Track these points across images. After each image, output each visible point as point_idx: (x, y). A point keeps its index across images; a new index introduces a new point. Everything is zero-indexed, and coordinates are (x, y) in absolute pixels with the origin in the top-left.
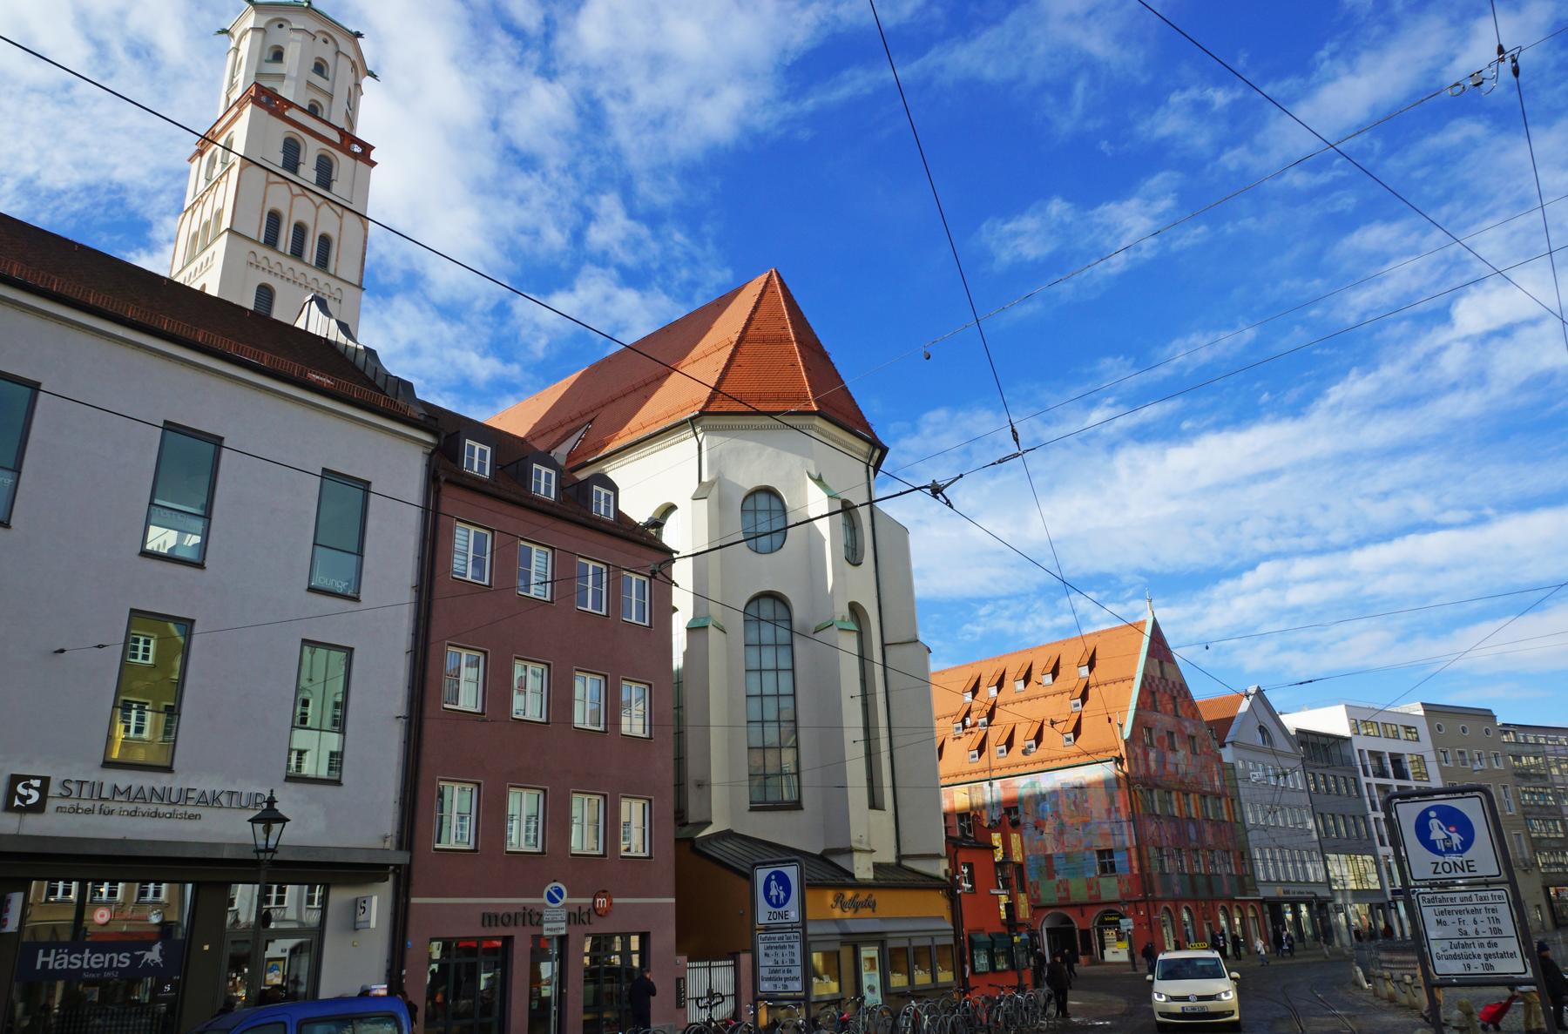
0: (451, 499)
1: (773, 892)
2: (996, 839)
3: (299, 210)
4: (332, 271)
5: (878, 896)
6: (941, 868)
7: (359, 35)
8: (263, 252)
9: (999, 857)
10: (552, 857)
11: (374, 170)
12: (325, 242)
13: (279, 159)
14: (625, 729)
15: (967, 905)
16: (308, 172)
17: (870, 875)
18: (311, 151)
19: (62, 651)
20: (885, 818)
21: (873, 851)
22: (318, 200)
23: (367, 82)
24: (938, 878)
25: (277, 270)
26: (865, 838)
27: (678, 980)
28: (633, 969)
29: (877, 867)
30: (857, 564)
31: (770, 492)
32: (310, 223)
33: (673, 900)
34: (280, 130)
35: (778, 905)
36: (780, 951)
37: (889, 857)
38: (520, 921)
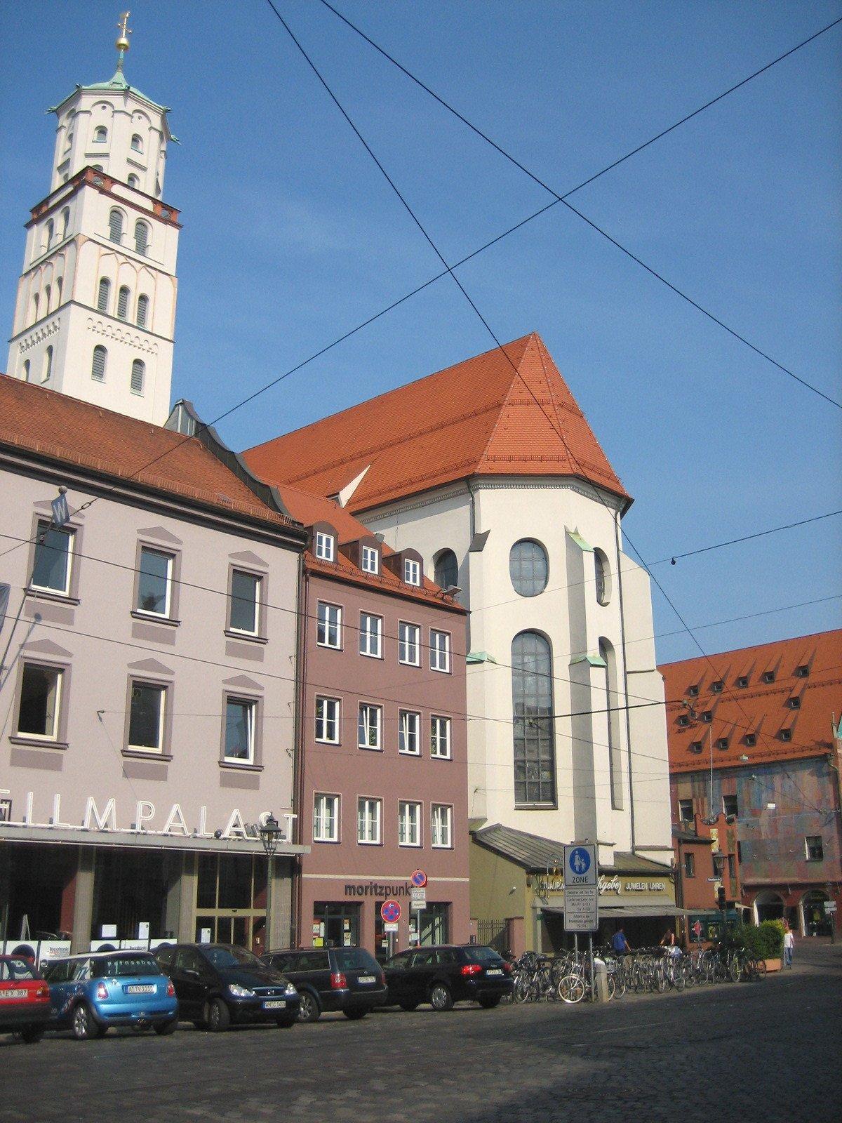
1: (577, 863)
6: (667, 858)
10: (388, 847)
13: (107, 232)
16: (129, 240)
22: (138, 266)
28: (175, 1012)
29: (617, 855)
32: (132, 287)
35: (580, 872)
37: (626, 848)
38: (369, 890)
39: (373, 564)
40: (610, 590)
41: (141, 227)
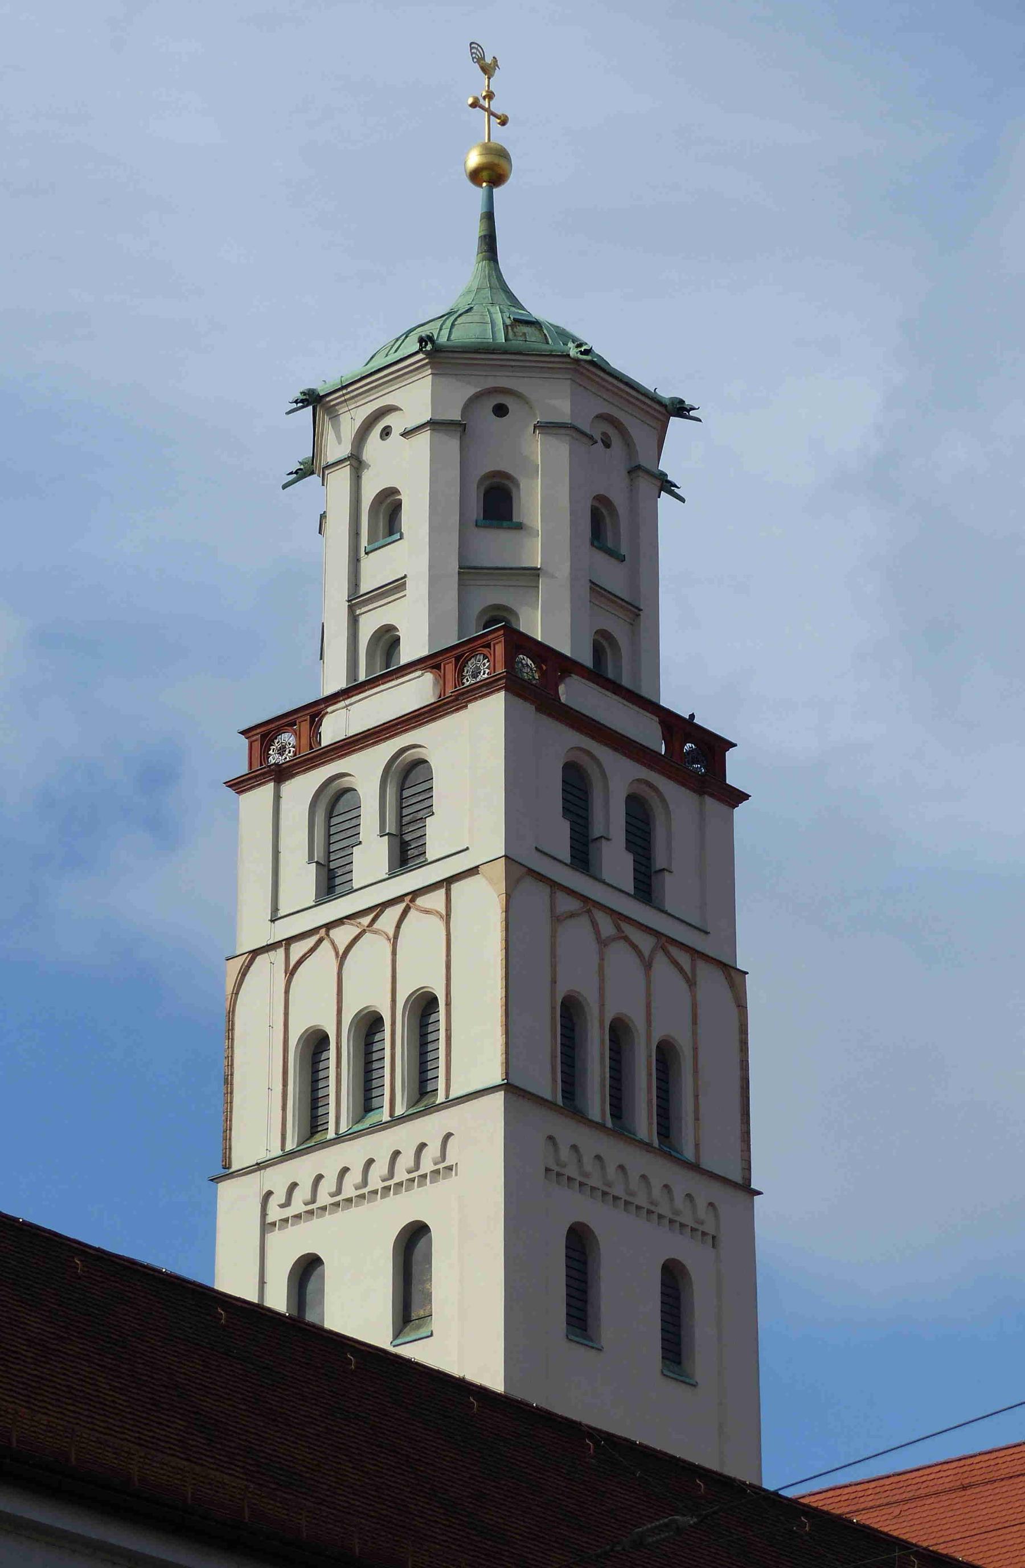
8: (568, 1132)
11: (740, 812)
12: (666, 1056)
16: (616, 862)
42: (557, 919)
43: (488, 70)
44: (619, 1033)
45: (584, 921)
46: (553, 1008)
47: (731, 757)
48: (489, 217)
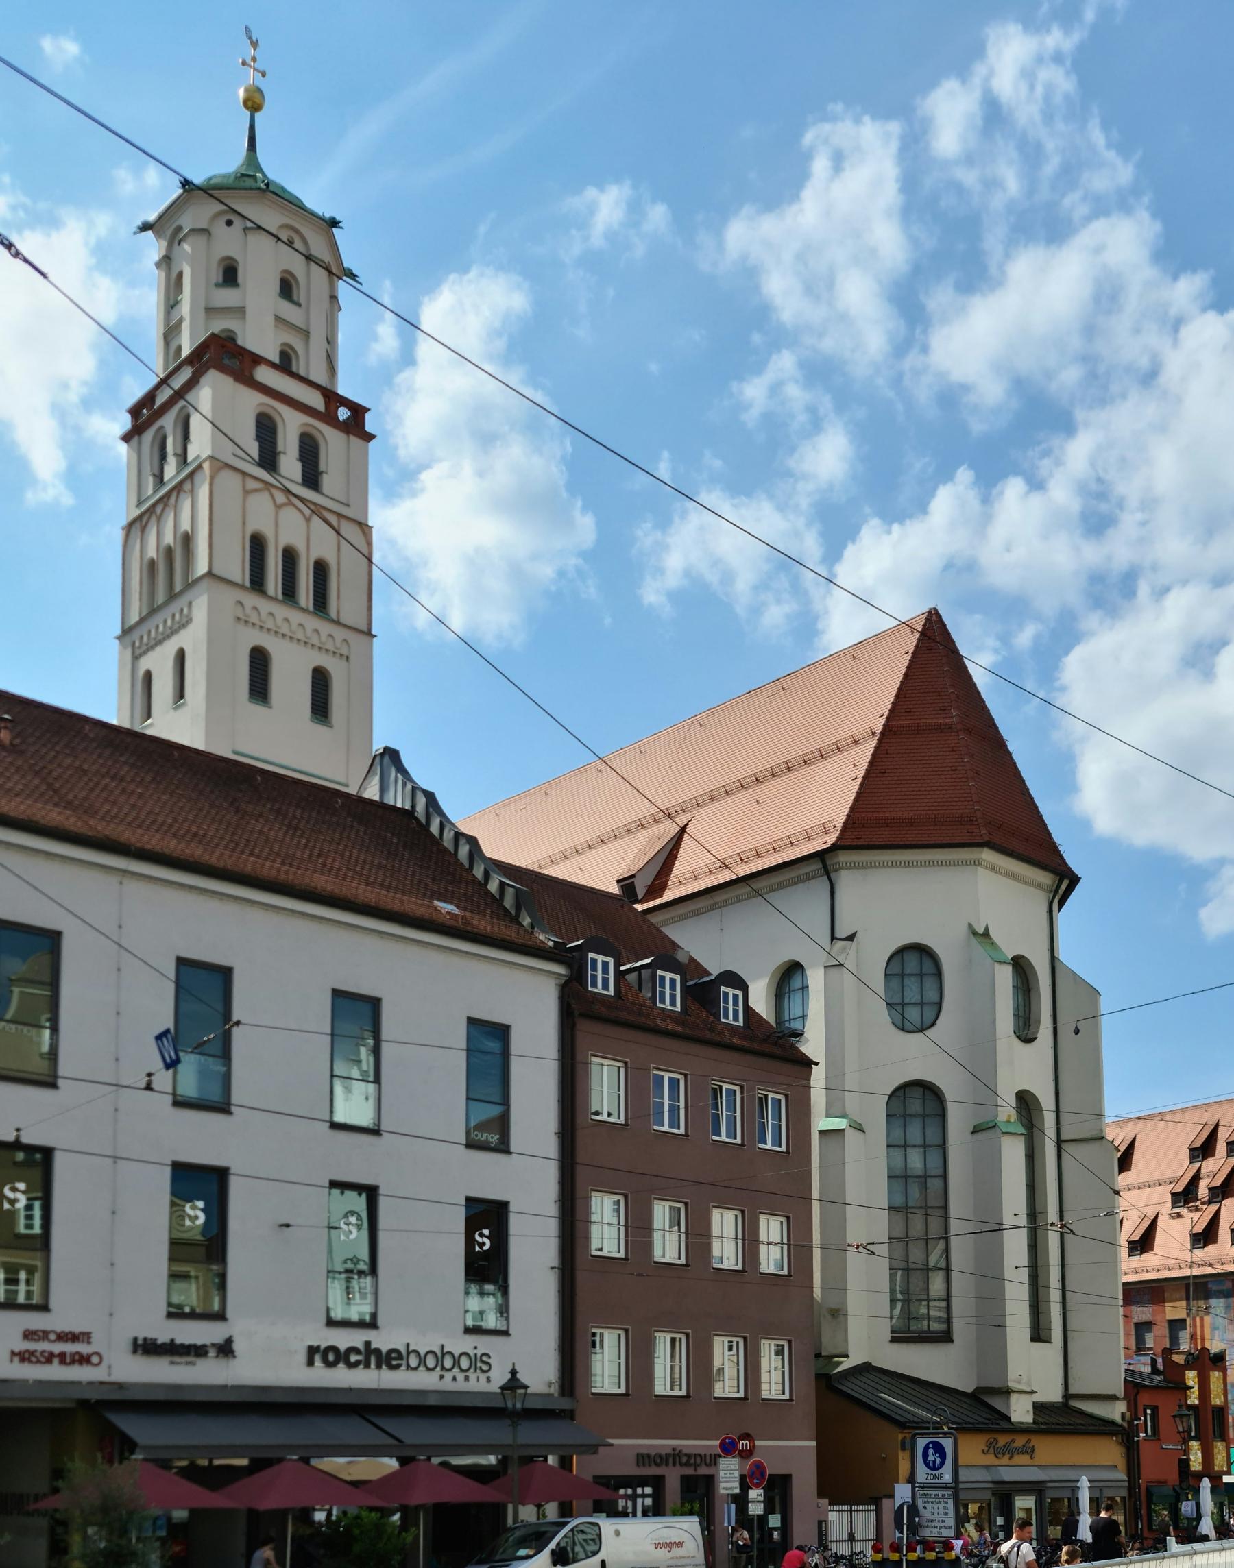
0: (585, 1029)
1: (931, 1458)
2: (1191, 1377)
3: (289, 529)
4: (333, 615)
5: (1036, 1441)
6: (1116, 1411)
7: (334, 223)
8: (251, 600)
9: (1194, 1399)
11: (372, 444)
12: (321, 569)
14: (763, 1268)
15: (1147, 1453)
16: (290, 465)
17: (1029, 1419)
18: (291, 426)
19: (288, 1226)
20: (1051, 1353)
21: (1033, 1392)
23: (343, 289)
24: (1112, 1423)
25: (270, 624)
26: (1024, 1379)
27: (820, 1523)
29: (1039, 1408)
30: (1029, 1040)
31: (922, 951)
33: (814, 1443)
34: (251, 401)
35: (935, 1468)
36: (935, 1505)
37: (1053, 1395)
38: (671, 1461)
39: (673, 997)
40: (1038, 1022)
41: (309, 451)
42: (247, 492)
43: (255, 45)
44: (290, 557)
45: (266, 495)
46: (244, 538)
47: (368, 416)
48: (252, 128)
